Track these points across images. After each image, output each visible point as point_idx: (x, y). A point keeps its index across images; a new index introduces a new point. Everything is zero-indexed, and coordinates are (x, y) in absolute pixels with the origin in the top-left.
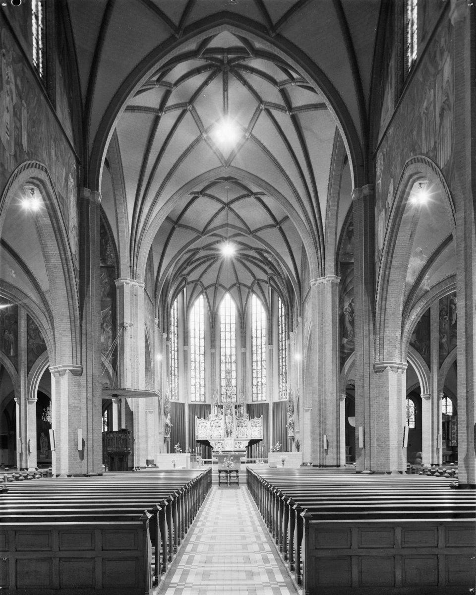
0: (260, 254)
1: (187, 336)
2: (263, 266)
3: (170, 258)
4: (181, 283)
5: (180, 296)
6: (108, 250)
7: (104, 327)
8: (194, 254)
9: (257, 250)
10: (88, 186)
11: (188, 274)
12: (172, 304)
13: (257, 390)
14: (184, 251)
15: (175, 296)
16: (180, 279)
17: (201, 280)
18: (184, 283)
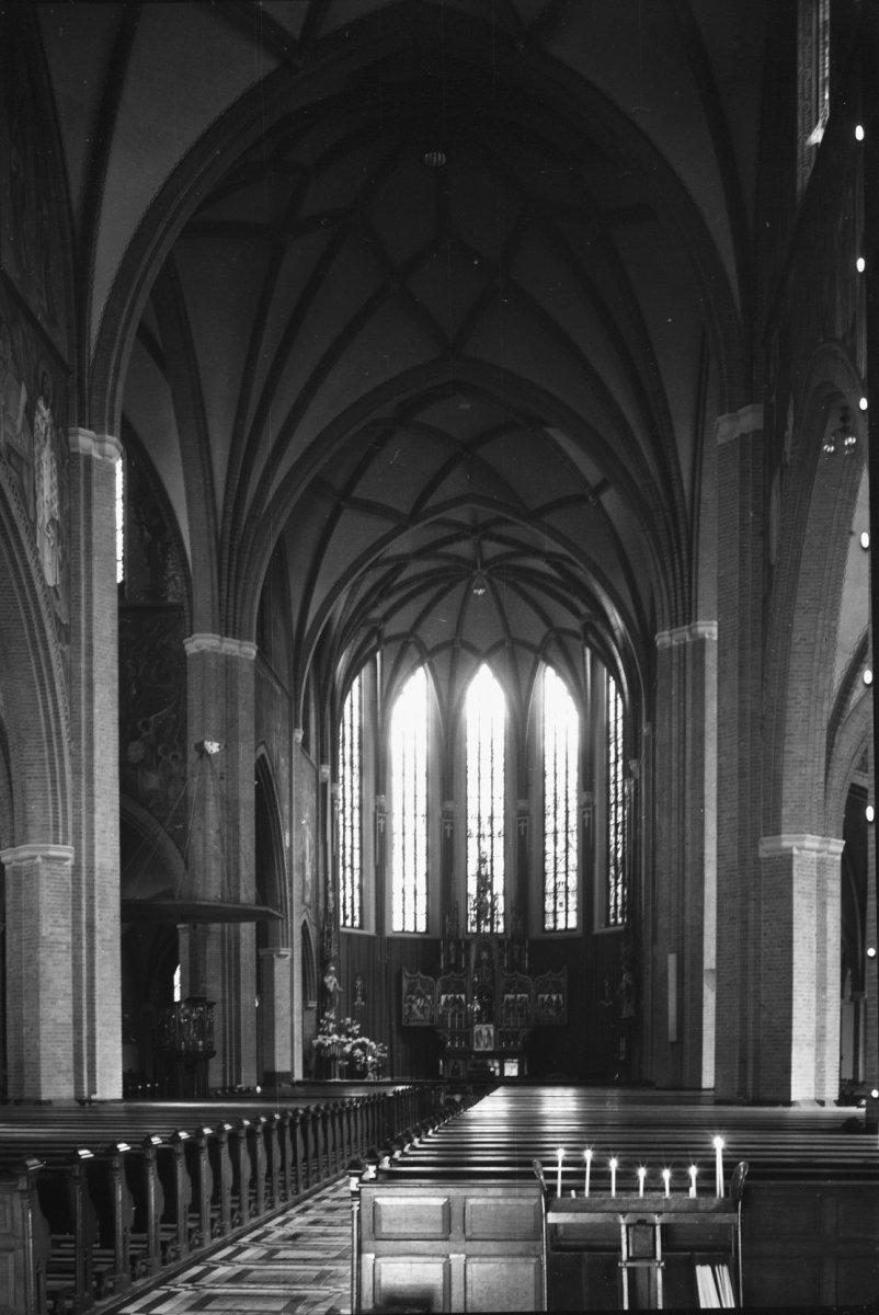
0: (555, 566)
1: (385, 768)
2: (568, 595)
3: (332, 582)
4: (366, 641)
5: (365, 672)
6: (170, 567)
7: (160, 754)
8: (397, 571)
9: (549, 557)
10: (87, 423)
11: (386, 618)
12: (347, 687)
13: (555, 903)
14: (365, 566)
15: (353, 671)
16: (363, 633)
17: (419, 632)
18: (374, 642)
